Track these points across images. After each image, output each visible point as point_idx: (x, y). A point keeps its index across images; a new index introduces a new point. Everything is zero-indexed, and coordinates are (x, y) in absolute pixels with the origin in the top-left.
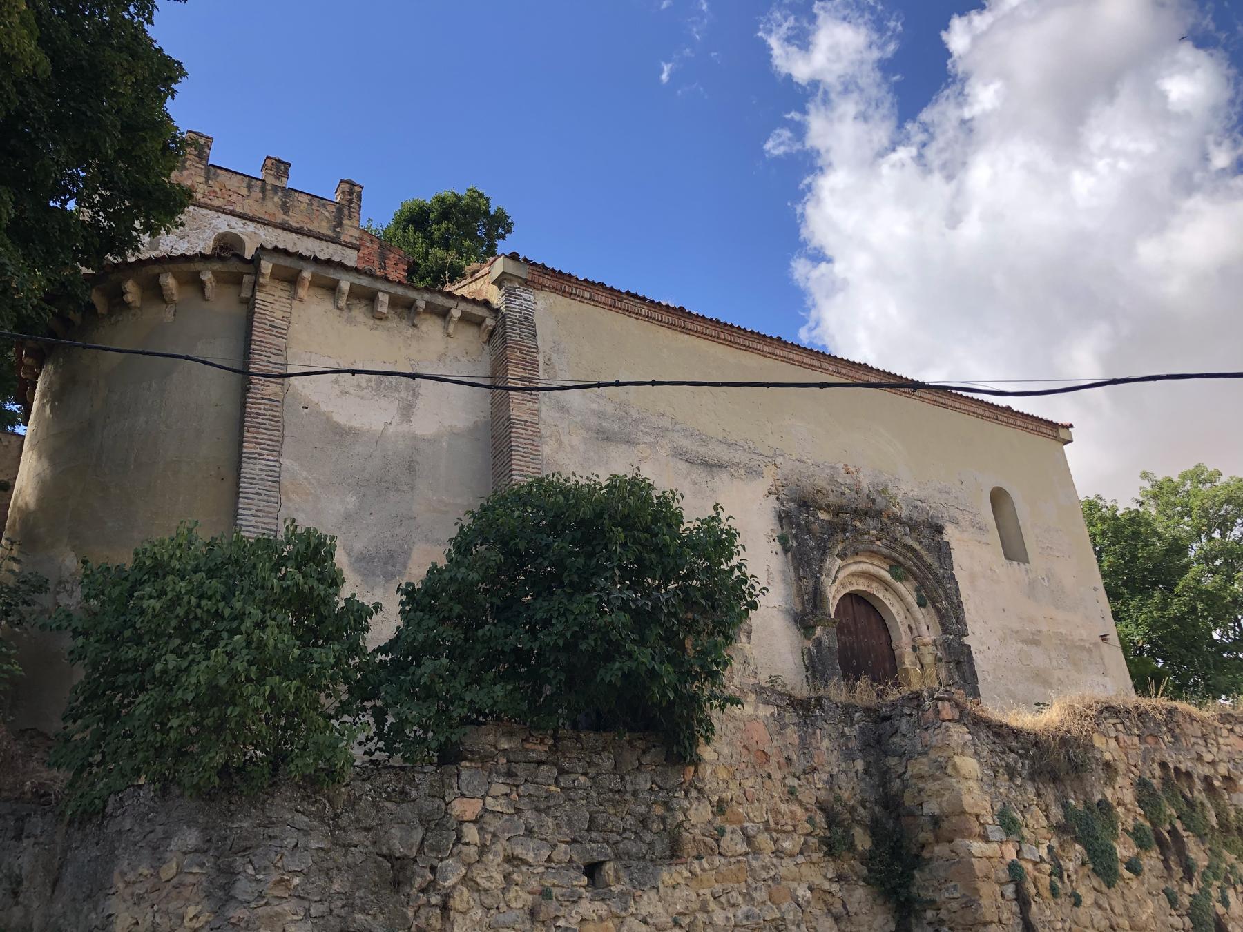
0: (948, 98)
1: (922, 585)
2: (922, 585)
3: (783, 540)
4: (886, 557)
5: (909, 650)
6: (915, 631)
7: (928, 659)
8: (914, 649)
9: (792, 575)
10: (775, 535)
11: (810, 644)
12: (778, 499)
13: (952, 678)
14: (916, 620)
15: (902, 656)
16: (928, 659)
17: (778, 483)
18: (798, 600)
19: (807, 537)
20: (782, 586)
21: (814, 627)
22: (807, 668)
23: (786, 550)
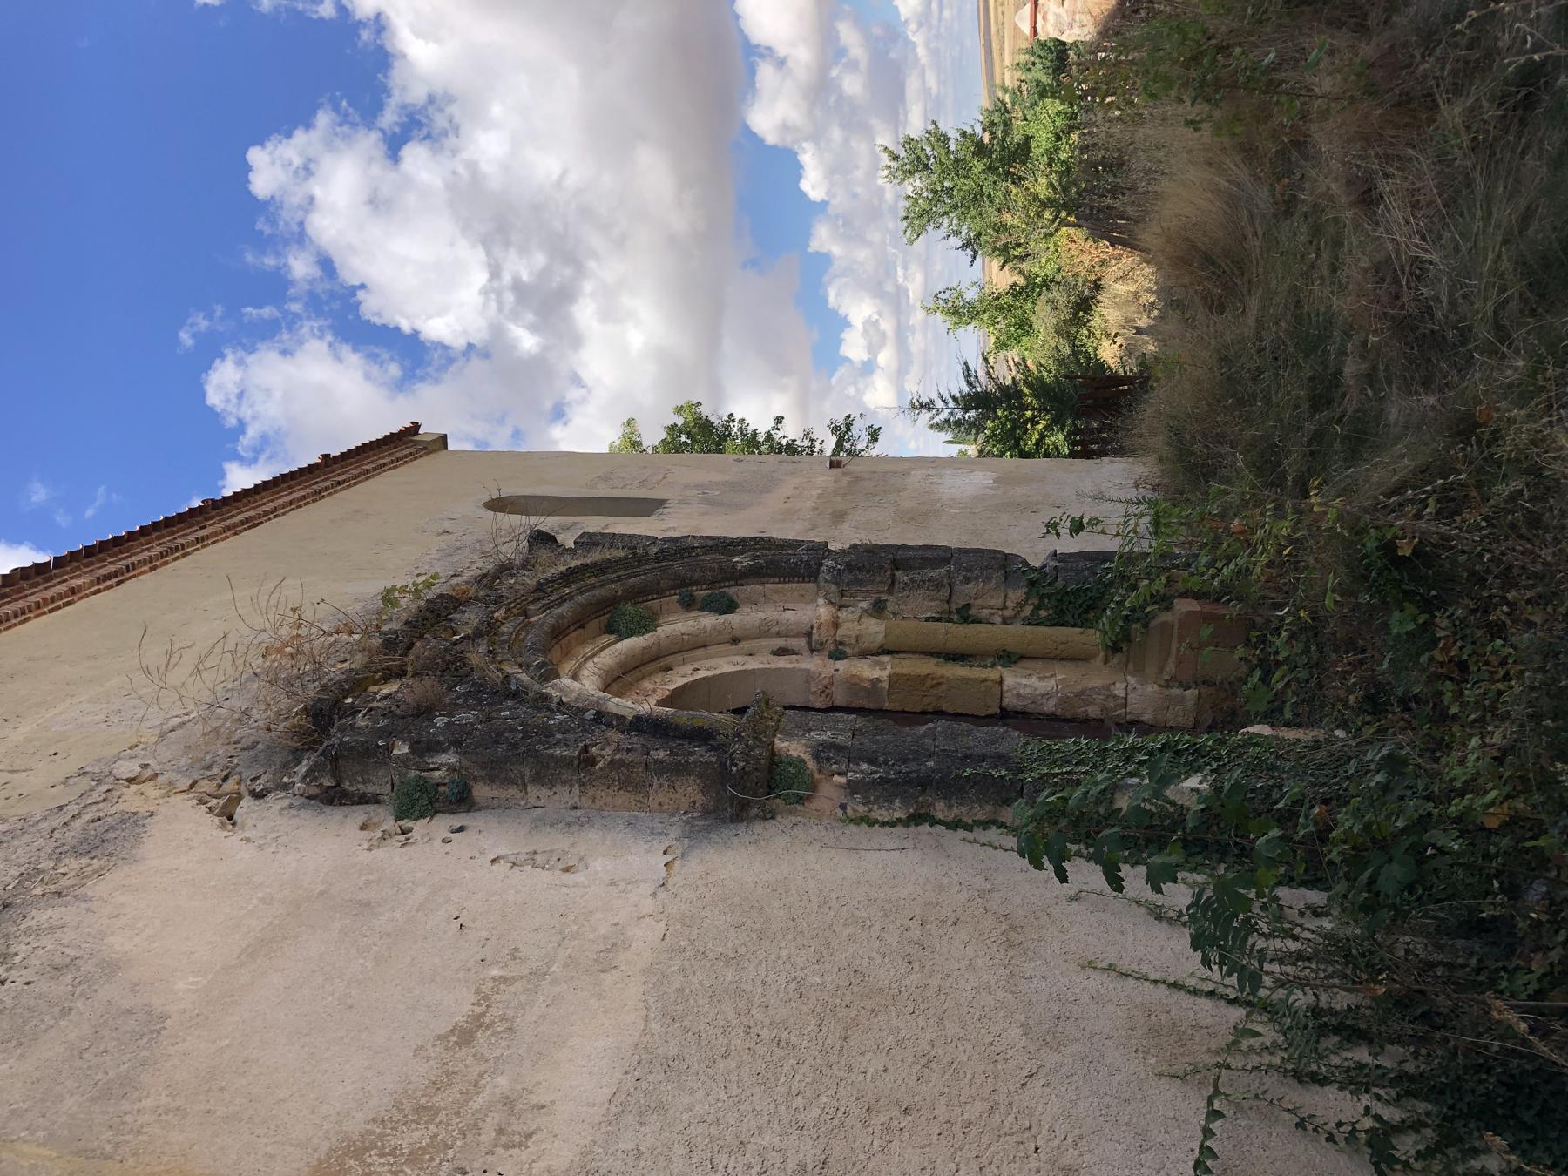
0: (134, 988)
1: (681, 583)
2: (681, 583)
3: (420, 802)
4: (580, 621)
5: (840, 665)
6: (794, 643)
7: (874, 629)
8: (838, 655)
9: (565, 795)
10: (390, 824)
11: (831, 789)
12: (258, 796)
13: (938, 585)
14: (764, 632)
15: (853, 684)
16: (874, 629)
17: (206, 786)
18: (659, 795)
19: (440, 722)
20: (593, 835)
21: (775, 761)
22: (916, 819)
23: (460, 800)
